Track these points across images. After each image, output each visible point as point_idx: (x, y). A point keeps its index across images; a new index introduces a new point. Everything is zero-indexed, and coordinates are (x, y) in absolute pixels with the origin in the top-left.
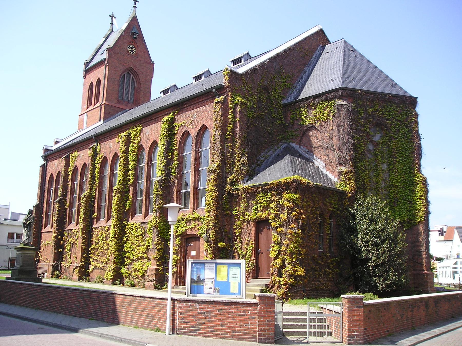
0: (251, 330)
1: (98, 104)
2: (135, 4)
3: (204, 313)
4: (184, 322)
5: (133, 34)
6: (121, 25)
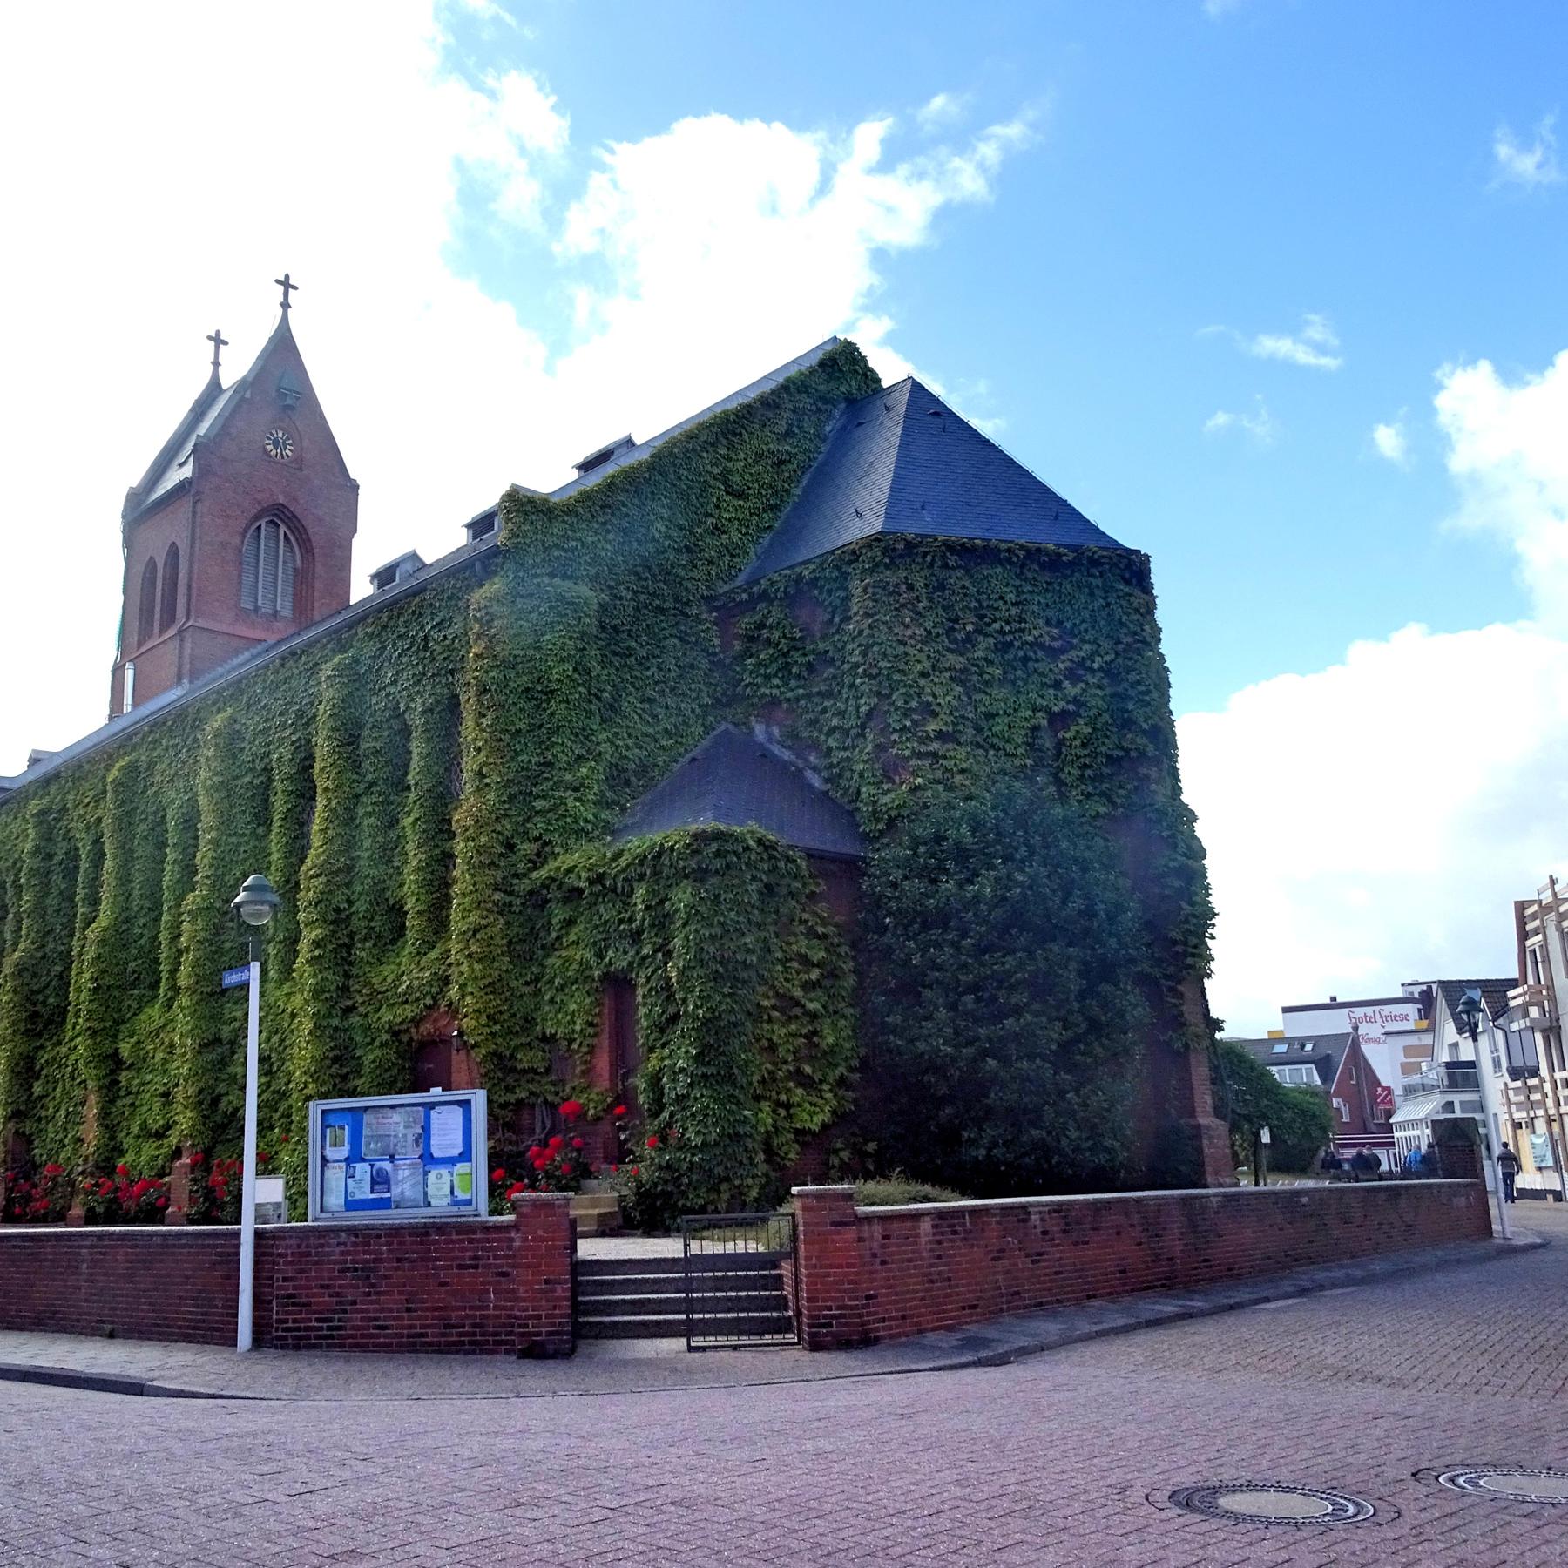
0: (498, 1317)
1: (172, 632)
2: (286, 295)
3: (356, 1270)
4: (294, 1304)
5: (280, 380)
6: (237, 366)
